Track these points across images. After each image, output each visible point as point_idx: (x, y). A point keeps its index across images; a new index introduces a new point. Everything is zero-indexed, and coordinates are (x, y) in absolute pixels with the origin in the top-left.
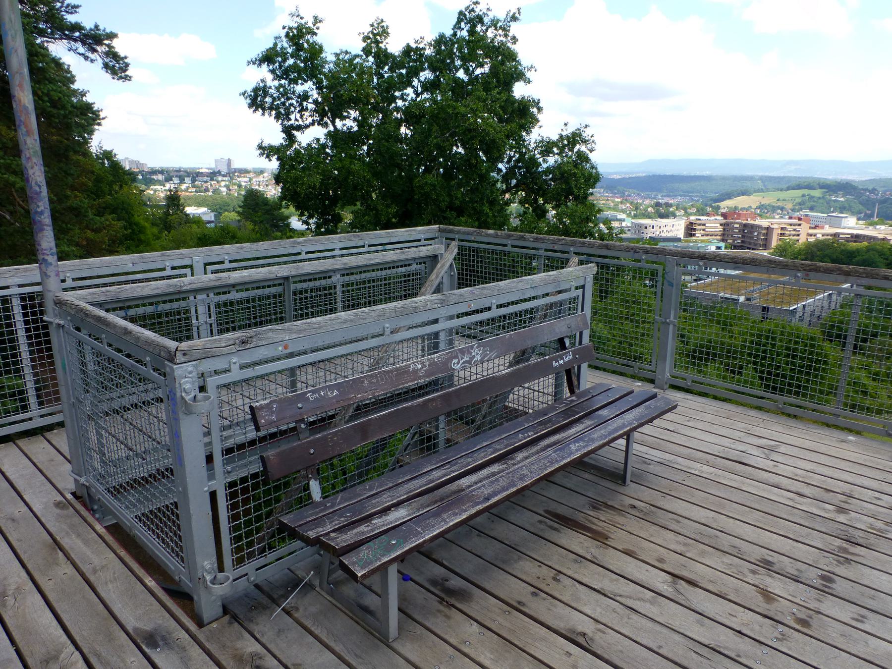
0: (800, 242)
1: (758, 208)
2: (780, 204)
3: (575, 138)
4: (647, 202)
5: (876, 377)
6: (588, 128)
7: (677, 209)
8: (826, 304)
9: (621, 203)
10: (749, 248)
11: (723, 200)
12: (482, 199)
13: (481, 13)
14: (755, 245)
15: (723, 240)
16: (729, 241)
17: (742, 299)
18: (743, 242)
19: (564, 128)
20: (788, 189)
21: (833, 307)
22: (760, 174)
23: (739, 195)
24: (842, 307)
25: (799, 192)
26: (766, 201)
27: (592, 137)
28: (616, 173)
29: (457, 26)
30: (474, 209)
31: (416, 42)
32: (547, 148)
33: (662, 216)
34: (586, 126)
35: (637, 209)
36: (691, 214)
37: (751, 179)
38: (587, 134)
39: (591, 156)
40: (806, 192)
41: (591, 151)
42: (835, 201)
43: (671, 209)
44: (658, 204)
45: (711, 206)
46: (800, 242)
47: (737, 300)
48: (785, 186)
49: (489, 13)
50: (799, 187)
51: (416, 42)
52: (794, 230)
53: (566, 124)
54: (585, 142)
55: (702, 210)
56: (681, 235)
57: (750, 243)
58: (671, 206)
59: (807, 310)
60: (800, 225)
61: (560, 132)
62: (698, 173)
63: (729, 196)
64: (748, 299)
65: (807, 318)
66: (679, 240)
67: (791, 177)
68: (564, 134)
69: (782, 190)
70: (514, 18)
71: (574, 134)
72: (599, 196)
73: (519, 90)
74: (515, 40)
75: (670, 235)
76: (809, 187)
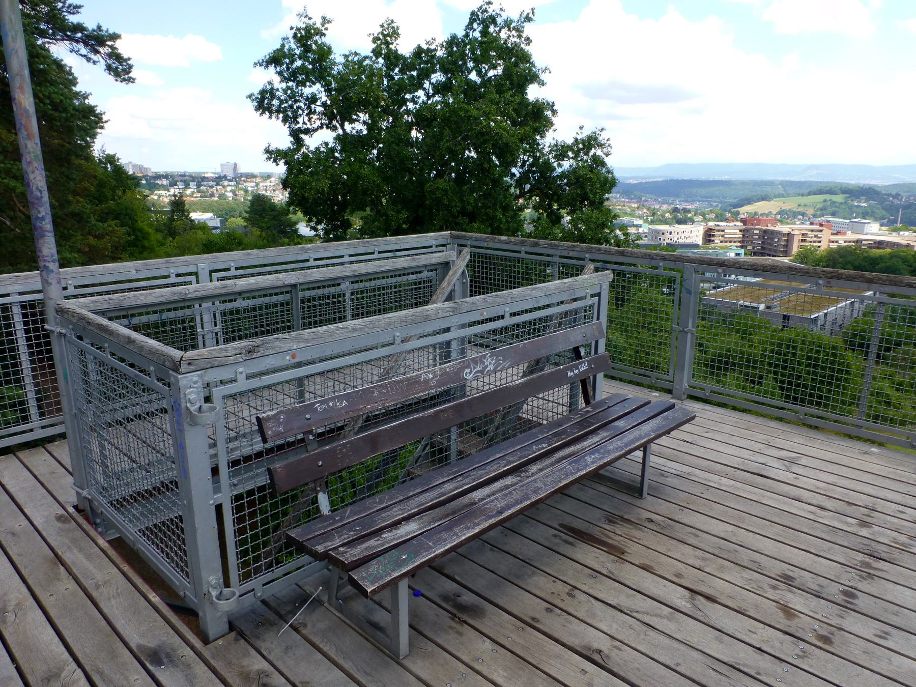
0: (822, 248)
1: (779, 213)
2: (801, 209)
3: (590, 142)
4: (665, 207)
5: (899, 387)
6: (604, 131)
7: (695, 215)
8: (848, 312)
9: (638, 208)
10: (769, 255)
11: (742, 206)
12: (495, 204)
13: (494, 14)
14: (776, 251)
15: (742, 247)
16: (749, 248)
17: (762, 307)
18: (763, 248)
19: (579, 131)
20: (810, 194)
21: (855, 315)
22: (781, 178)
23: (759, 201)
24: (864, 315)
25: (820, 198)
26: (786, 207)
27: (608, 140)
28: (632, 178)
29: (470, 27)
30: (487, 214)
31: (427, 43)
32: (562, 152)
33: (680, 222)
34: (602, 130)
35: (654, 214)
36: (710, 220)
37: (771, 183)
38: (602, 137)
39: (607, 160)
40: (828, 197)
41: (607, 155)
42: (858, 206)
43: (689, 215)
44: (676, 210)
45: (730, 212)
46: (822, 248)
47: (757, 308)
48: (806, 191)
49: (502, 13)
50: (820, 192)
51: (427, 43)
52: (816, 236)
53: (581, 128)
54: (601, 145)
55: (721, 215)
56: (699, 241)
57: (770, 250)
58: (689, 211)
59: (829, 318)
60: (821, 231)
61: (575, 135)
62: (717, 178)
63: (749, 201)
64: (768, 307)
65: (828, 327)
66: (697, 246)
67: (812, 182)
68: (579, 137)
69: (803, 195)
70: (528, 19)
71: (590, 138)
72: (615, 201)
73: (533, 93)
74: (528, 41)
75: (688, 241)
76: (831, 192)
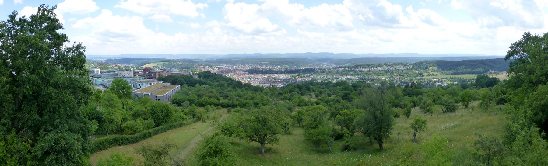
0: (164, 76)
1: (153, 67)
2: (158, 66)
3: (78, 47)
4: (123, 66)
5: (186, 114)
6: (82, 44)
7: (131, 68)
8: (172, 93)
9: (115, 66)
10: (151, 79)
11: (143, 65)
12: (41, 68)
13: (46, 8)
14: (153, 77)
15: (144, 77)
16: (146, 77)
17: (150, 94)
18: (149, 77)
19: (74, 43)
20: (160, 62)
21: (174, 94)
22: (152, 58)
23: (147, 64)
24: (176, 94)
25: (162, 63)
26: (154, 65)
27: (85, 46)
28: (113, 58)
29: (38, 12)
30: (38, 72)
31: (23, 17)
32: (69, 50)
33: (127, 70)
34: (82, 43)
35: (120, 68)
36: (135, 69)
37: (150, 59)
38: (83, 45)
39: (85, 53)
40: (164, 62)
41: (85, 51)
42: (171, 65)
43: (129, 68)
44: (125, 67)
45: (140, 67)
46: (164, 76)
47: (149, 94)
48: (159, 61)
49: (48, 7)
50: (162, 61)
51: (23, 17)
52: (162, 73)
53: (75, 42)
54: (82, 48)
55: (138, 68)
56: (132, 75)
57: (151, 77)
58: (129, 67)
59: (167, 96)
60: (163, 71)
61: (73, 45)
62: (136, 58)
63: (145, 64)
64: (151, 94)
65: (167, 98)
66: (132, 77)
67: (174, 59)
68: (75, 45)
69: (158, 62)
70: (54, 8)
71: (78, 45)
72: (86, 66)
73: (60, 32)
74: (55, 15)
75: (129, 76)
76: (165, 61)
